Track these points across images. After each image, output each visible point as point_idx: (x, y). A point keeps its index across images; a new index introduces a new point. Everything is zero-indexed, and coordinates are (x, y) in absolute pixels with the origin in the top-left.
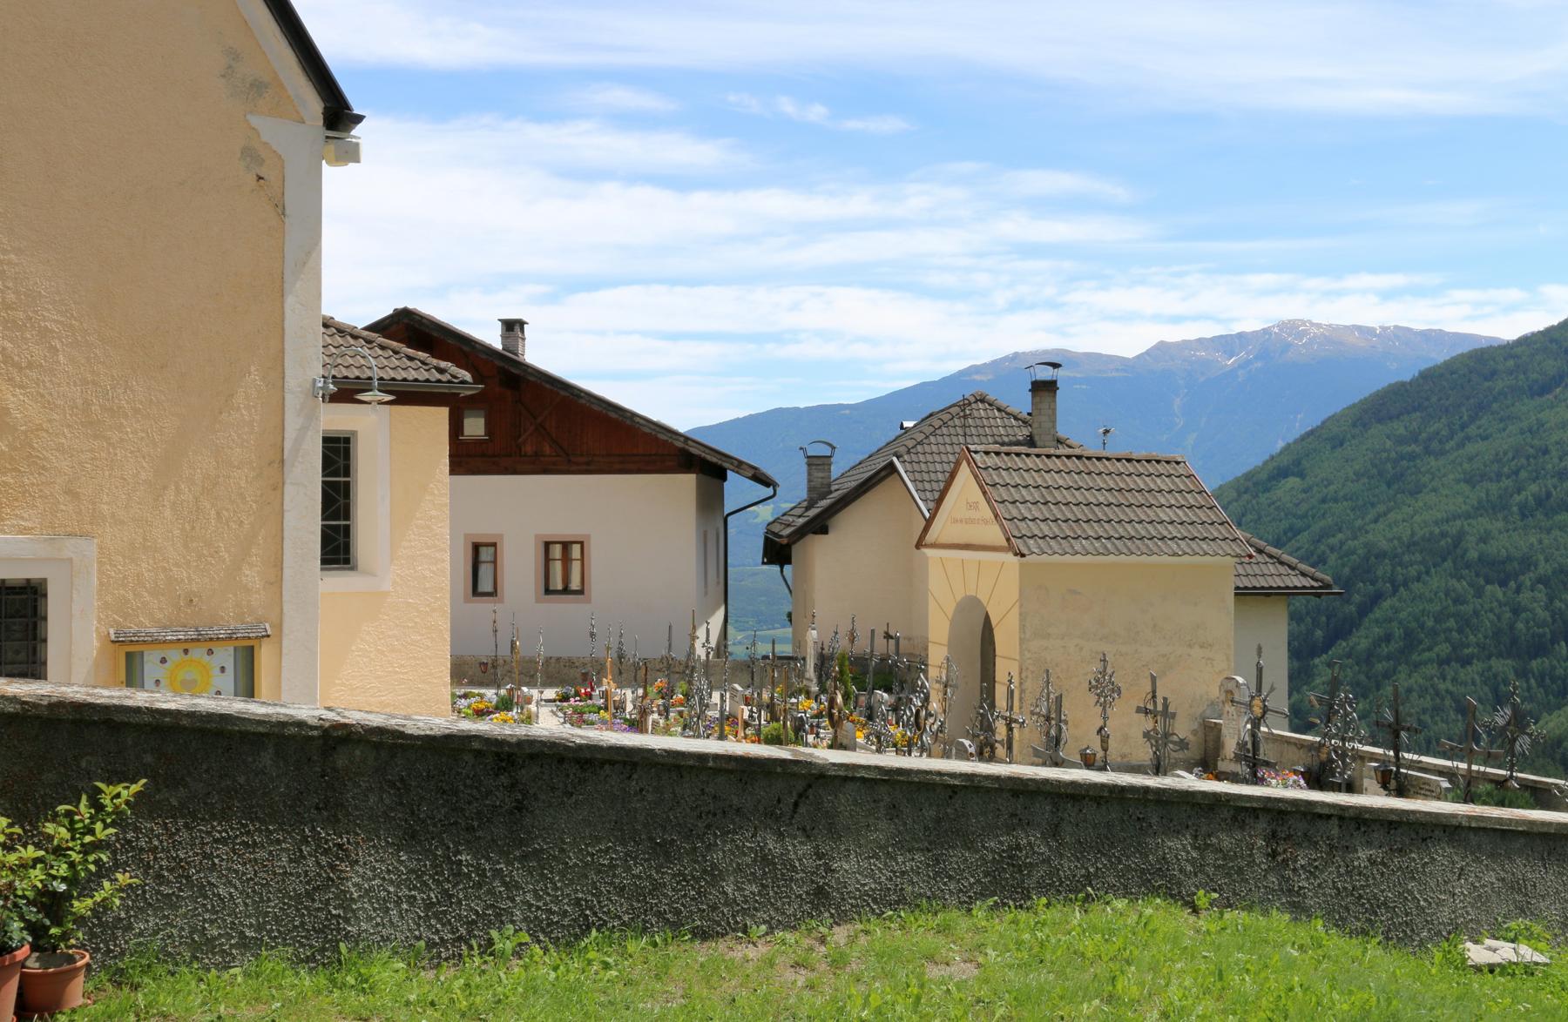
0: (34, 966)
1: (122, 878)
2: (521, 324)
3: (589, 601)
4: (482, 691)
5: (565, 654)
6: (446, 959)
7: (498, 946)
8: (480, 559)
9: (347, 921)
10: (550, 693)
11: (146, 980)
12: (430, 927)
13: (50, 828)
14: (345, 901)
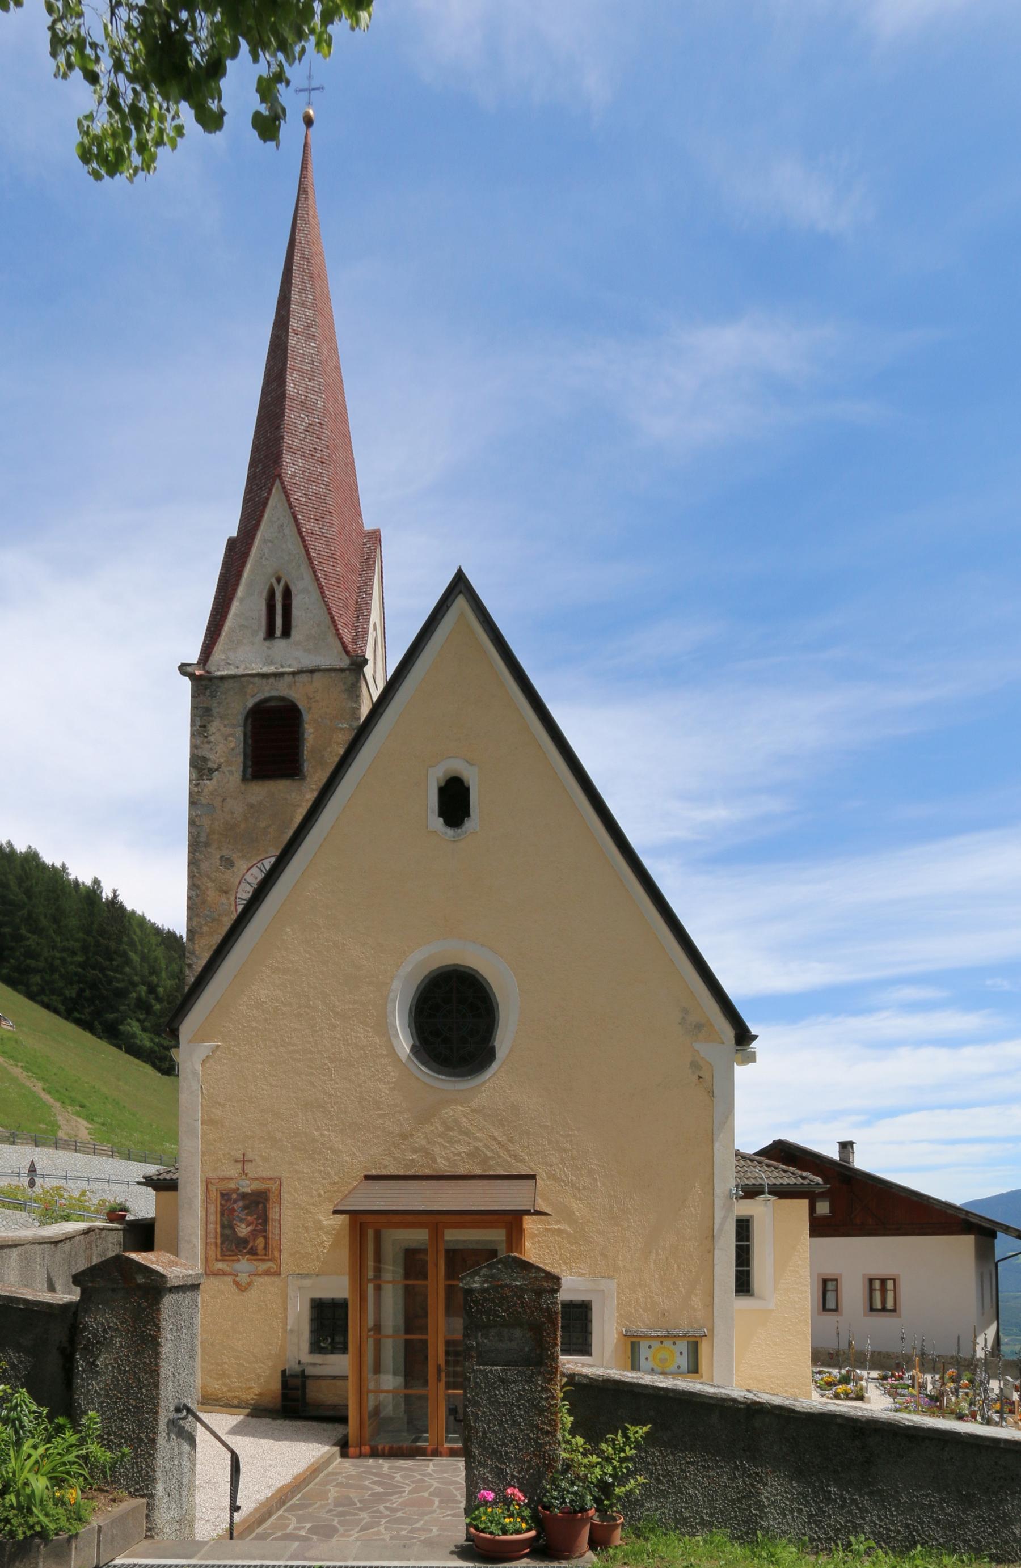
0: (597, 1520)
1: (641, 1479)
2: (851, 1144)
3: (900, 1316)
4: (830, 1370)
5: (884, 1349)
6: (822, 1550)
7: (855, 1547)
8: (828, 1290)
9: (761, 1518)
10: (875, 1374)
11: (652, 1536)
12: (811, 1529)
13: (604, 1446)
14: (761, 1507)
